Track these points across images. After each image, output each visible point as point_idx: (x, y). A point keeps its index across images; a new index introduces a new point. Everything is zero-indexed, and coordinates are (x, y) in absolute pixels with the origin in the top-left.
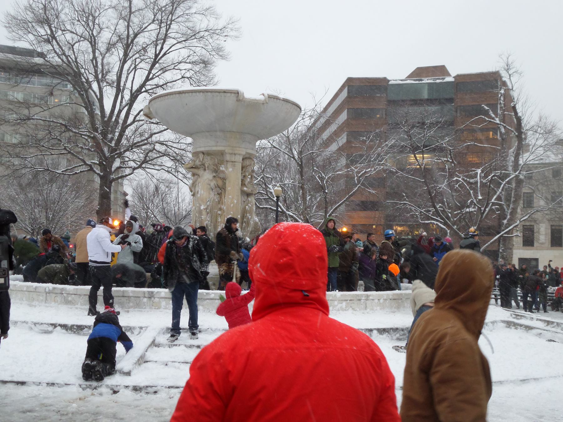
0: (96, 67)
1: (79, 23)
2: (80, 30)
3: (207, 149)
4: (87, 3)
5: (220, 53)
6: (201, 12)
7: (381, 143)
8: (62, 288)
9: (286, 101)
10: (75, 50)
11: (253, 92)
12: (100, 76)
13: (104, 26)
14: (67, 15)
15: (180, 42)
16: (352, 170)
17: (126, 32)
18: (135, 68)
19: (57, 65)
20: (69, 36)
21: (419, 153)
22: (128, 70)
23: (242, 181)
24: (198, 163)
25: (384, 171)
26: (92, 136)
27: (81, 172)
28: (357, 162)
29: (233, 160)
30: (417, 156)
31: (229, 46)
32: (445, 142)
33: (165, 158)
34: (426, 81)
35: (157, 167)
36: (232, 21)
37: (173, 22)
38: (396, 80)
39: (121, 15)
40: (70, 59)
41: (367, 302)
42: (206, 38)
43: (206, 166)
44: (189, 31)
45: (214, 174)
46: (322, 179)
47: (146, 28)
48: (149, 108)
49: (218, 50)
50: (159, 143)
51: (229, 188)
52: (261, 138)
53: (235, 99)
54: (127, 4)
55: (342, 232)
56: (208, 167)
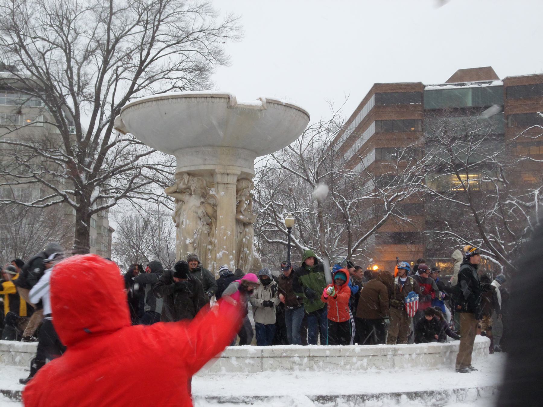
0: (70, 78)
1: (52, 28)
2: (52, 36)
3: (193, 168)
4: (61, 5)
5: (219, 58)
6: (195, 10)
7: (415, 161)
8: (10, 345)
9: (289, 106)
10: (46, 60)
11: (247, 96)
12: (76, 89)
13: (80, 31)
14: (37, 18)
15: (170, 45)
16: (381, 194)
17: (106, 37)
18: (117, 80)
19: (26, 78)
20: (39, 44)
21: (463, 172)
22: (109, 81)
23: (238, 207)
24: (182, 186)
25: (421, 193)
26: (67, 160)
27: (54, 203)
28: (386, 184)
29: (226, 181)
30: (461, 176)
31: (229, 48)
32: (493, 158)
33: (154, 185)
34: (470, 85)
35: (145, 196)
36: (231, 19)
37: (161, 23)
38: (433, 86)
39: (100, 17)
40: (41, 71)
41: (396, 358)
42: (201, 40)
43: (192, 189)
44: (181, 32)
45: (202, 200)
46: (344, 205)
47: (129, 30)
48: (121, 121)
49: (216, 54)
50: (146, 167)
51: (220, 217)
52: (259, 153)
53: (225, 105)
54: (107, 5)
55: (372, 271)
56: (194, 191)
